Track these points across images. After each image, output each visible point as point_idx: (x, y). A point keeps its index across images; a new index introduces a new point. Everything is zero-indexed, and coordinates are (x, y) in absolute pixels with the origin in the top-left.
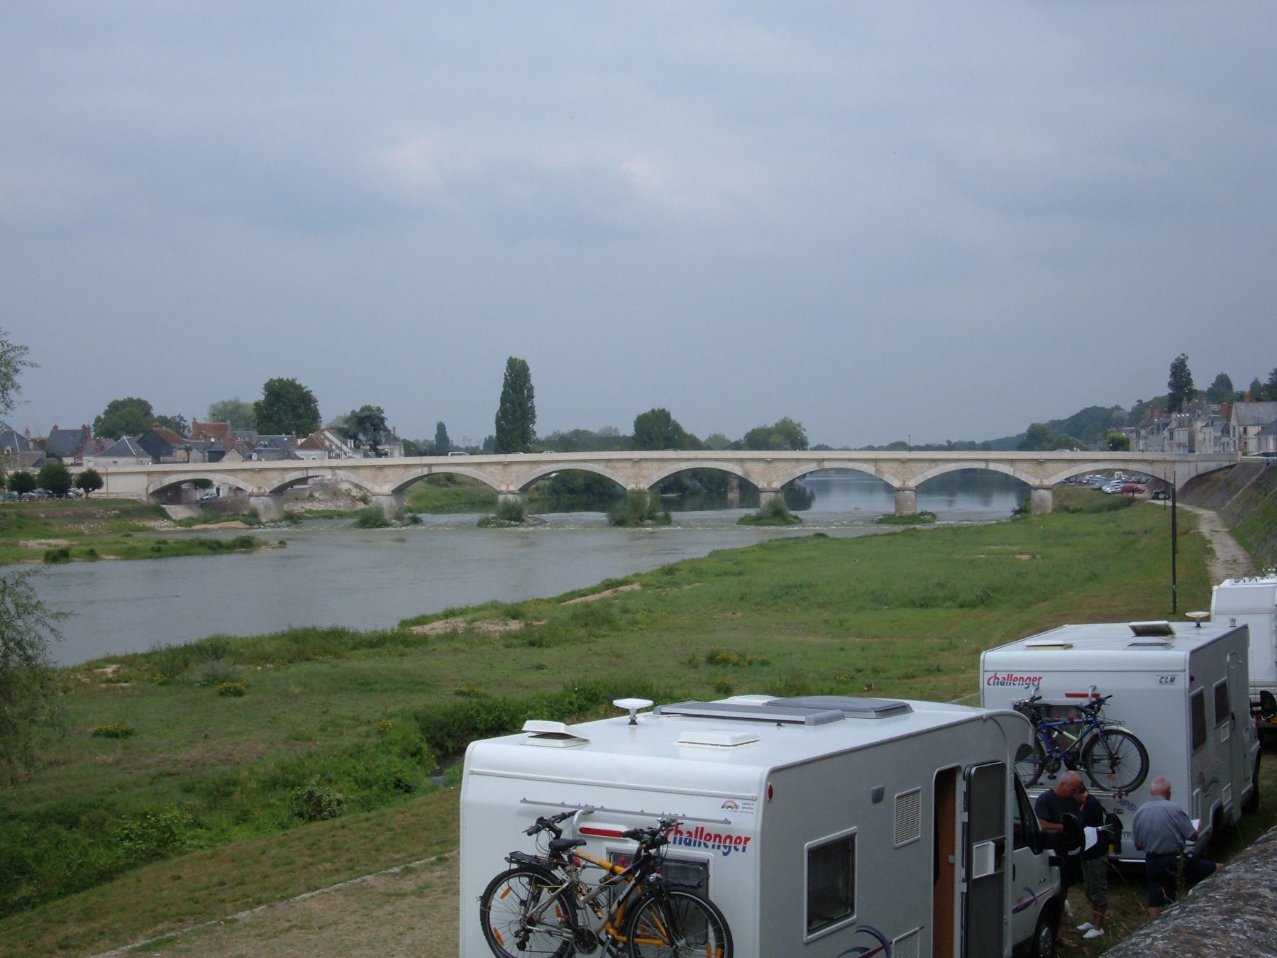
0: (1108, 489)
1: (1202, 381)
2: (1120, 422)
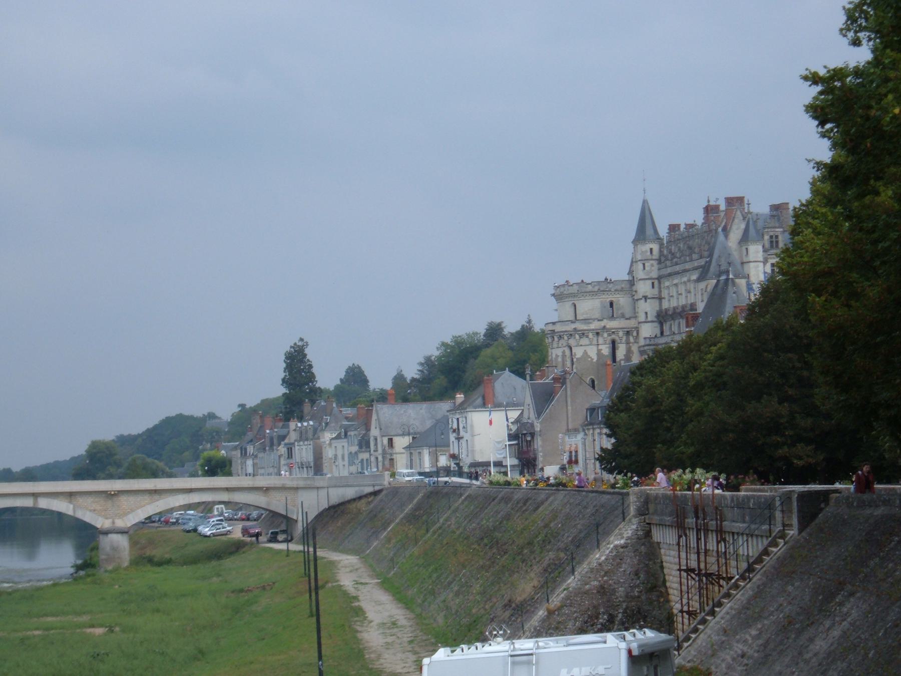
0: (206, 530)
1: (327, 376)
2: (215, 437)
